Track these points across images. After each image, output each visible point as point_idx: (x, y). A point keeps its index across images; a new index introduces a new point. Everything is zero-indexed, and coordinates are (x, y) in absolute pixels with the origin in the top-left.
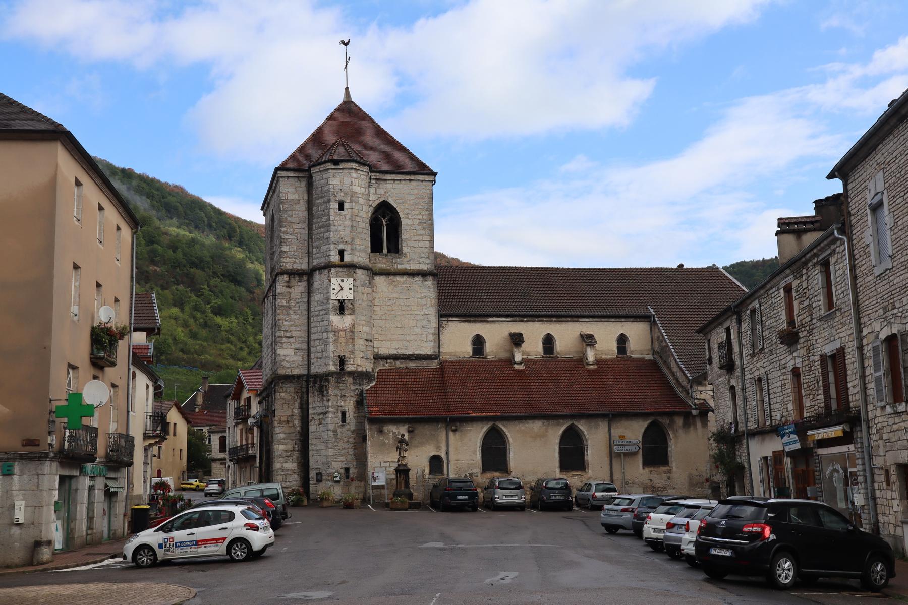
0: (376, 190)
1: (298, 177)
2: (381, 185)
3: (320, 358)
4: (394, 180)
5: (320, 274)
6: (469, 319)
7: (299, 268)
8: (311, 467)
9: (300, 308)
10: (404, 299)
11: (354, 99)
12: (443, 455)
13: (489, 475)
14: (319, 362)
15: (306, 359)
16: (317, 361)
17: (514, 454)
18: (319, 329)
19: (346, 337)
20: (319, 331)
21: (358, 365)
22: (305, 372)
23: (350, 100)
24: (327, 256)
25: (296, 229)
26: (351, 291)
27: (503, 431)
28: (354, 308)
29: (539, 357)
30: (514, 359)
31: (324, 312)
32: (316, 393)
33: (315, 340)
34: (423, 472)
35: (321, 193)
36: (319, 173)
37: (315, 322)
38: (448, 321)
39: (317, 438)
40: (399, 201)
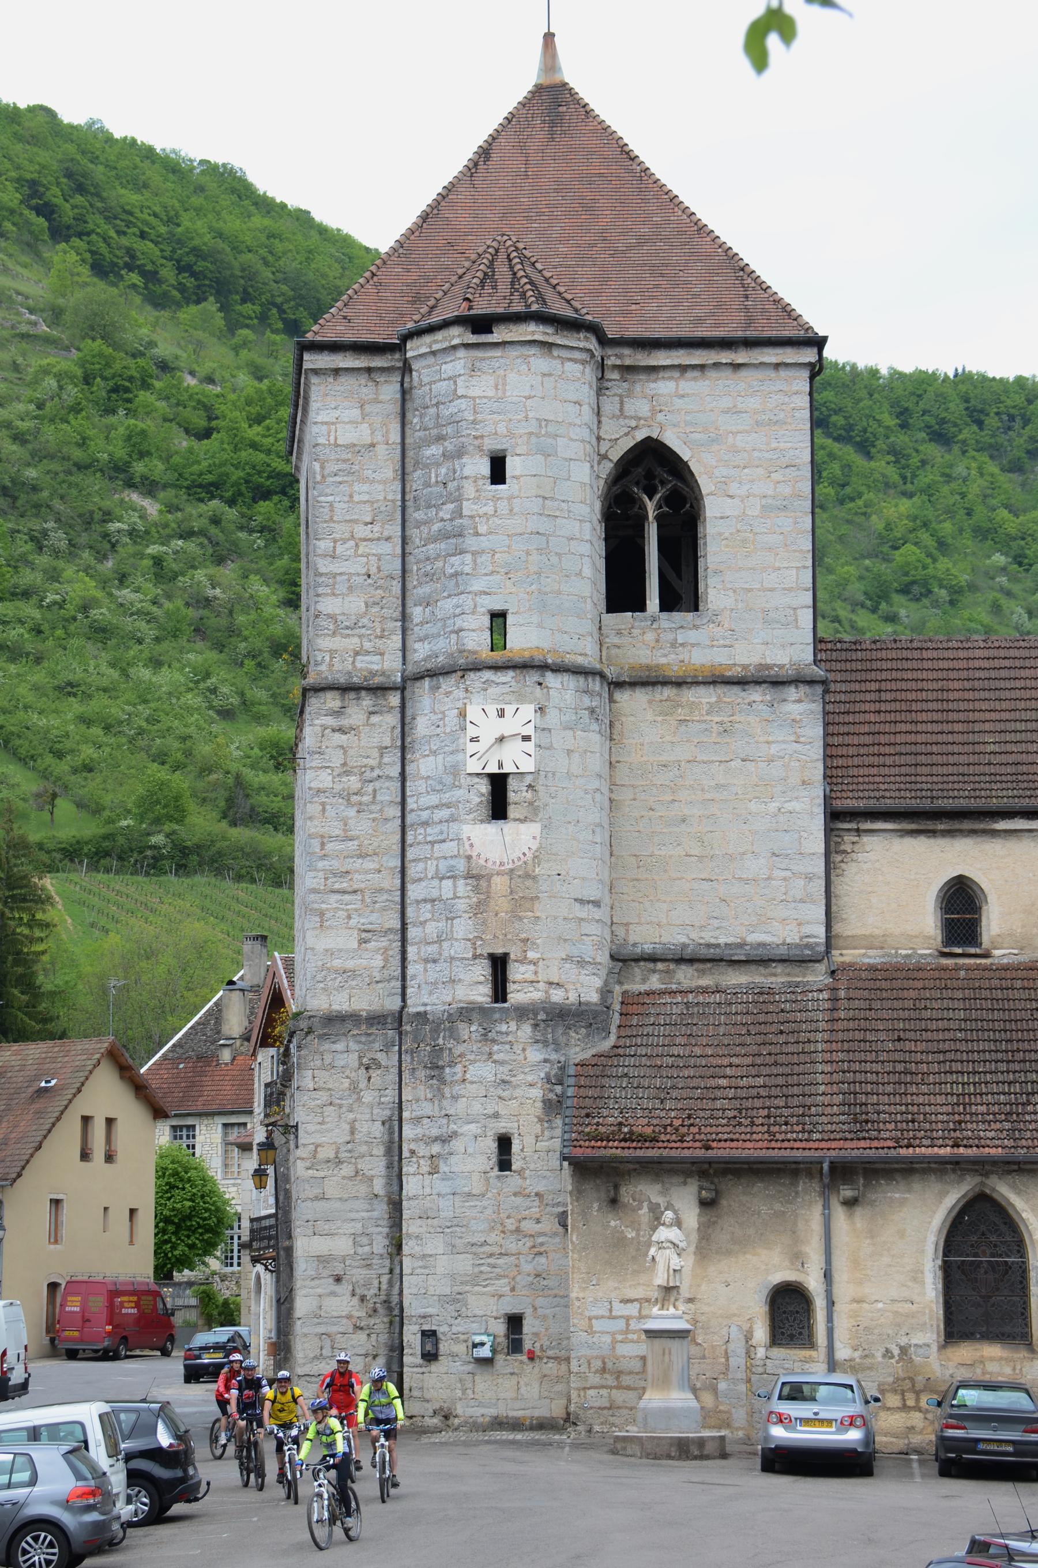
0: (622, 403)
2: (638, 388)
3: (435, 961)
4: (683, 368)
6: (930, 825)
7: (375, 667)
9: (379, 798)
11: (573, 74)
12: (814, 1284)
13: (965, 1352)
14: (434, 973)
16: (426, 970)
19: (511, 893)
21: (551, 983)
23: (557, 79)
24: (452, 632)
25: (365, 540)
31: (445, 813)
32: (422, 1074)
33: (418, 902)
34: (748, 1336)
35: (438, 426)
36: (431, 360)
37: (419, 843)
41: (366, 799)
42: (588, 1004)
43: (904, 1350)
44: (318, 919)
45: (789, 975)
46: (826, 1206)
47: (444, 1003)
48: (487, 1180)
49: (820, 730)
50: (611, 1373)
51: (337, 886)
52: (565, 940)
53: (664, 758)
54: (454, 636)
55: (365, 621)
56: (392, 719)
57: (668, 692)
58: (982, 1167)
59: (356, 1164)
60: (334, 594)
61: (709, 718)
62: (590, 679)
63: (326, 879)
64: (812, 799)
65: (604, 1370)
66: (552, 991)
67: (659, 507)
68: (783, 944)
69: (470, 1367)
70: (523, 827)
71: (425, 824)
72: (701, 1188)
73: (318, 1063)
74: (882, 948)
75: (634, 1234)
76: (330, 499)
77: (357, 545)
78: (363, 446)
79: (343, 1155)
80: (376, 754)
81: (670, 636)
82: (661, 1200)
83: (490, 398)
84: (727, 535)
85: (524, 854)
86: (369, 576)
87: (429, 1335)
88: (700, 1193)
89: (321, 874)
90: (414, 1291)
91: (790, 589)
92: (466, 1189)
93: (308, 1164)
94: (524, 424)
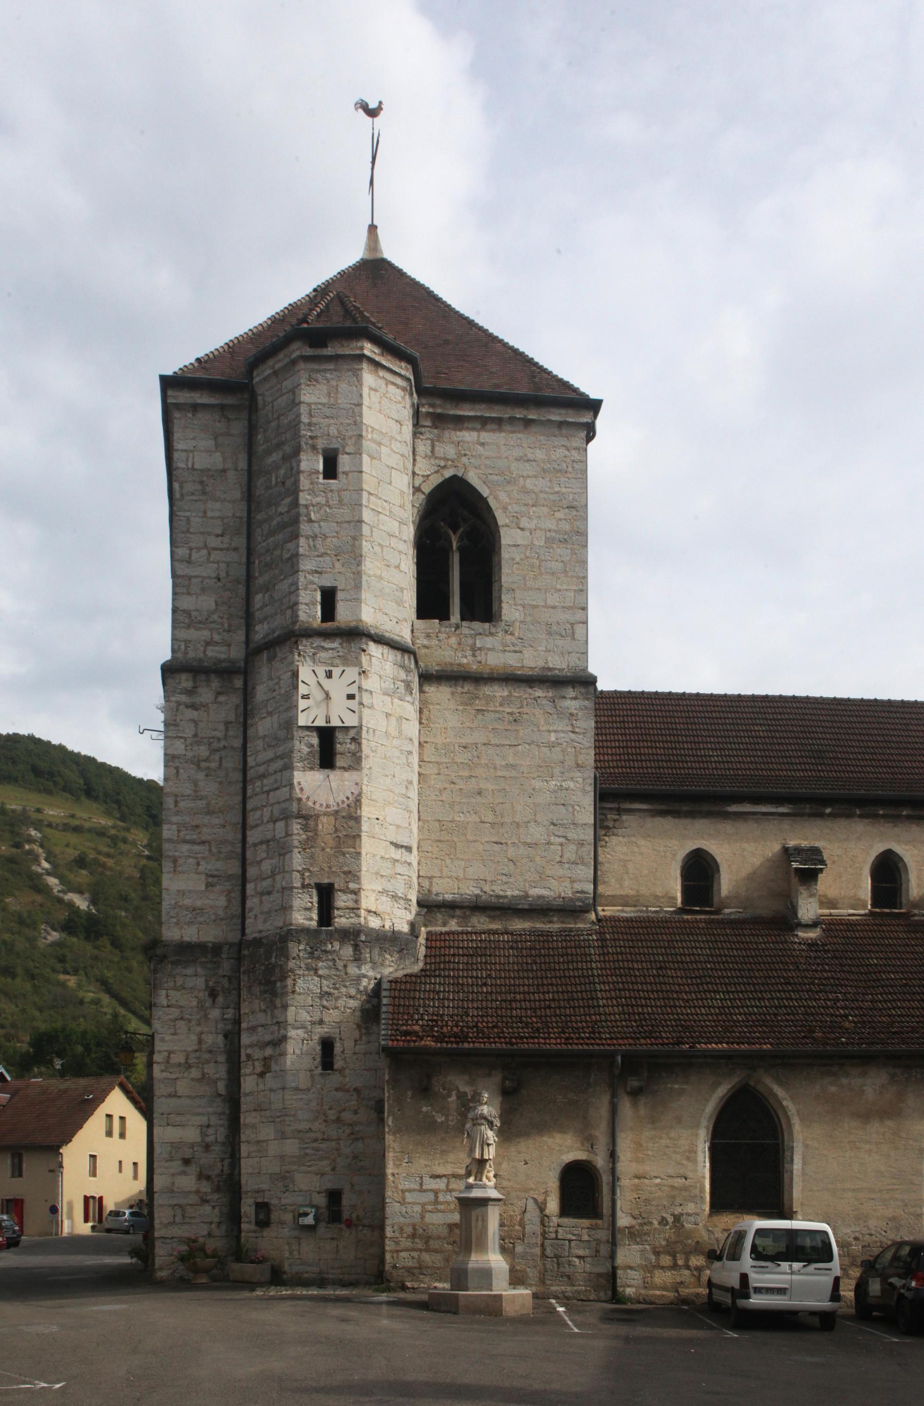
0: (433, 446)
1: (222, 408)
3: (269, 893)
5: (271, 659)
7: (223, 656)
8: (244, 1189)
9: (224, 764)
10: (503, 745)
12: (600, 1161)
13: (730, 1221)
15: (236, 903)
16: (261, 902)
17: (804, 1163)
18: (267, 812)
19: (336, 831)
20: (265, 820)
21: (370, 911)
22: (234, 937)
23: (379, 256)
25: (215, 549)
26: (353, 704)
27: (775, 1096)
28: (360, 750)
29: (862, 912)
30: (795, 914)
31: (278, 764)
32: (257, 990)
33: (255, 845)
34: (542, 1207)
38: (619, 811)
39: (258, 1109)
40: (495, 478)
41: (213, 765)
42: (400, 932)
43: (677, 1218)
44: (171, 865)
45: (563, 922)
46: (614, 1095)
47: (277, 928)
48: (312, 1076)
49: (593, 725)
50: (420, 1237)
51: (188, 837)
52: (382, 876)
53: (464, 741)
54: (289, 612)
55: (215, 617)
56: (235, 700)
57: (468, 687)
58: (753, 1061)
59: (203, 1068)
60: (189, 594)
61: (501, 709)
62: (406, 657)
63: (179, 831)
64: (584, 779)
65: (413, 1236)
66: (369, 918)
67: (461, 539)
68: (559, 897)
69: (296, 1233)
70: (346, 774)
71: (263, 776)
72: (504, 1079)
73: (171, 984)
74: (635, 906)
75: (443, 1119)
76: (188, 514)
77: (209, 554)
78: (216, 471)
79: (192, 1061)
80: (222, 727)
81: (470, 641)
82: (468, 1090)
83: (324, 405)
84: (518, 560)
85: (348, 798)
86: (219, 580)
87: (263, 1207)
88: (503, 1083)
89: (175, 827)
90: (250, 1171)
91: (569, 608)
92: (294, 1085)
93: (163, 1068)
94: (354, 427)
